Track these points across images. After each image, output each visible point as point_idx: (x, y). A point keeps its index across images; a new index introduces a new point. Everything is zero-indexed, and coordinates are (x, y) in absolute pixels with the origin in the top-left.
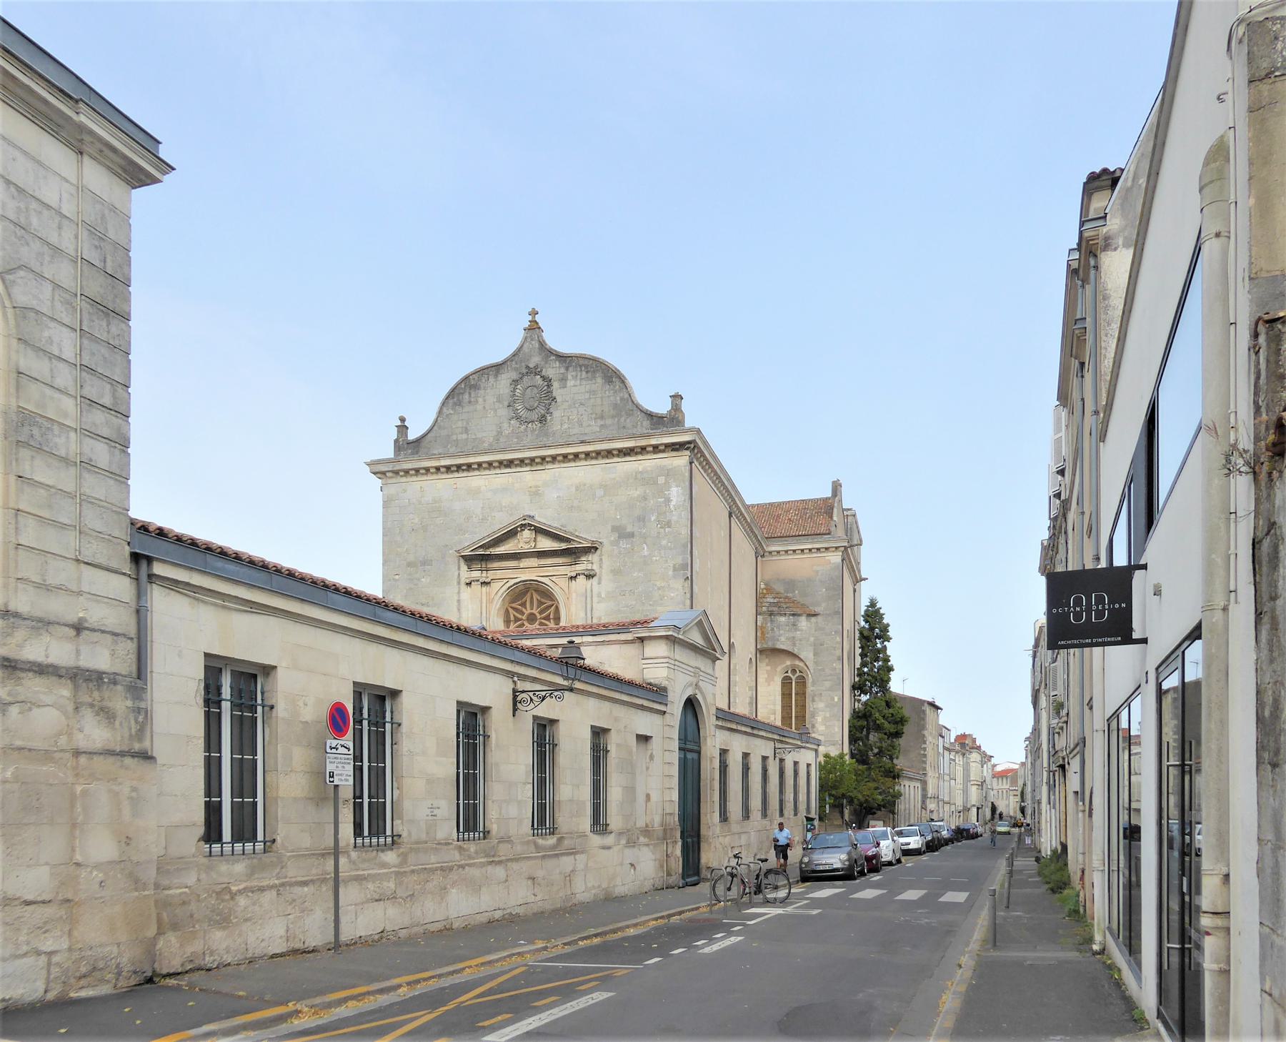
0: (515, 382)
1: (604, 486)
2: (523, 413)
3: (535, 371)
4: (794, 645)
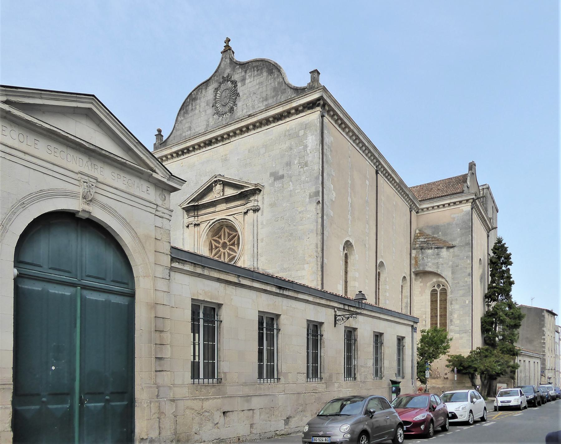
0: (216, 90)
1: (265, 146)
2: (220, 109)
3: (227, 79)
4: (438, 267)
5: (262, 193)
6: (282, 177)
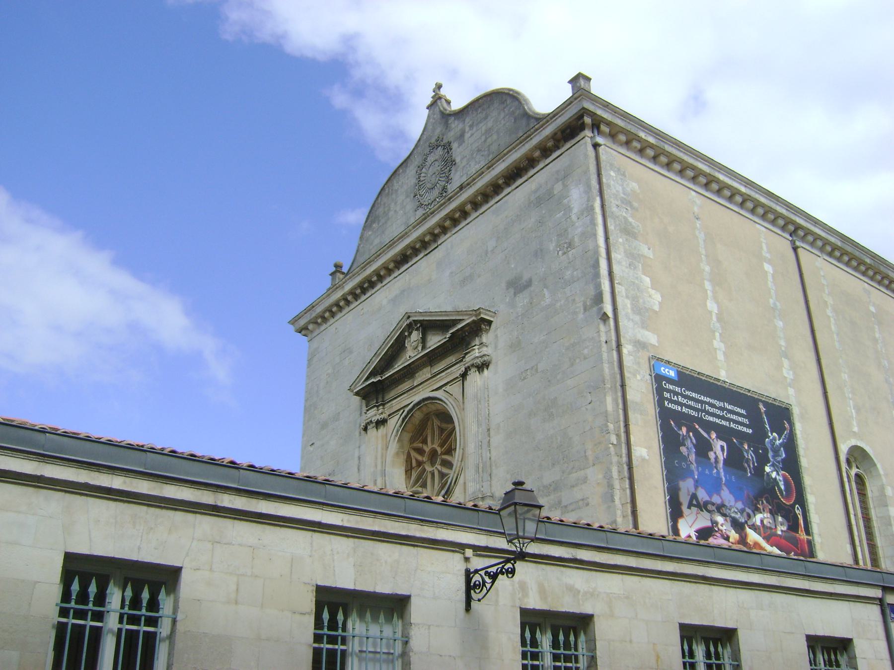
5: (493, 326)
6: (529, 283)
